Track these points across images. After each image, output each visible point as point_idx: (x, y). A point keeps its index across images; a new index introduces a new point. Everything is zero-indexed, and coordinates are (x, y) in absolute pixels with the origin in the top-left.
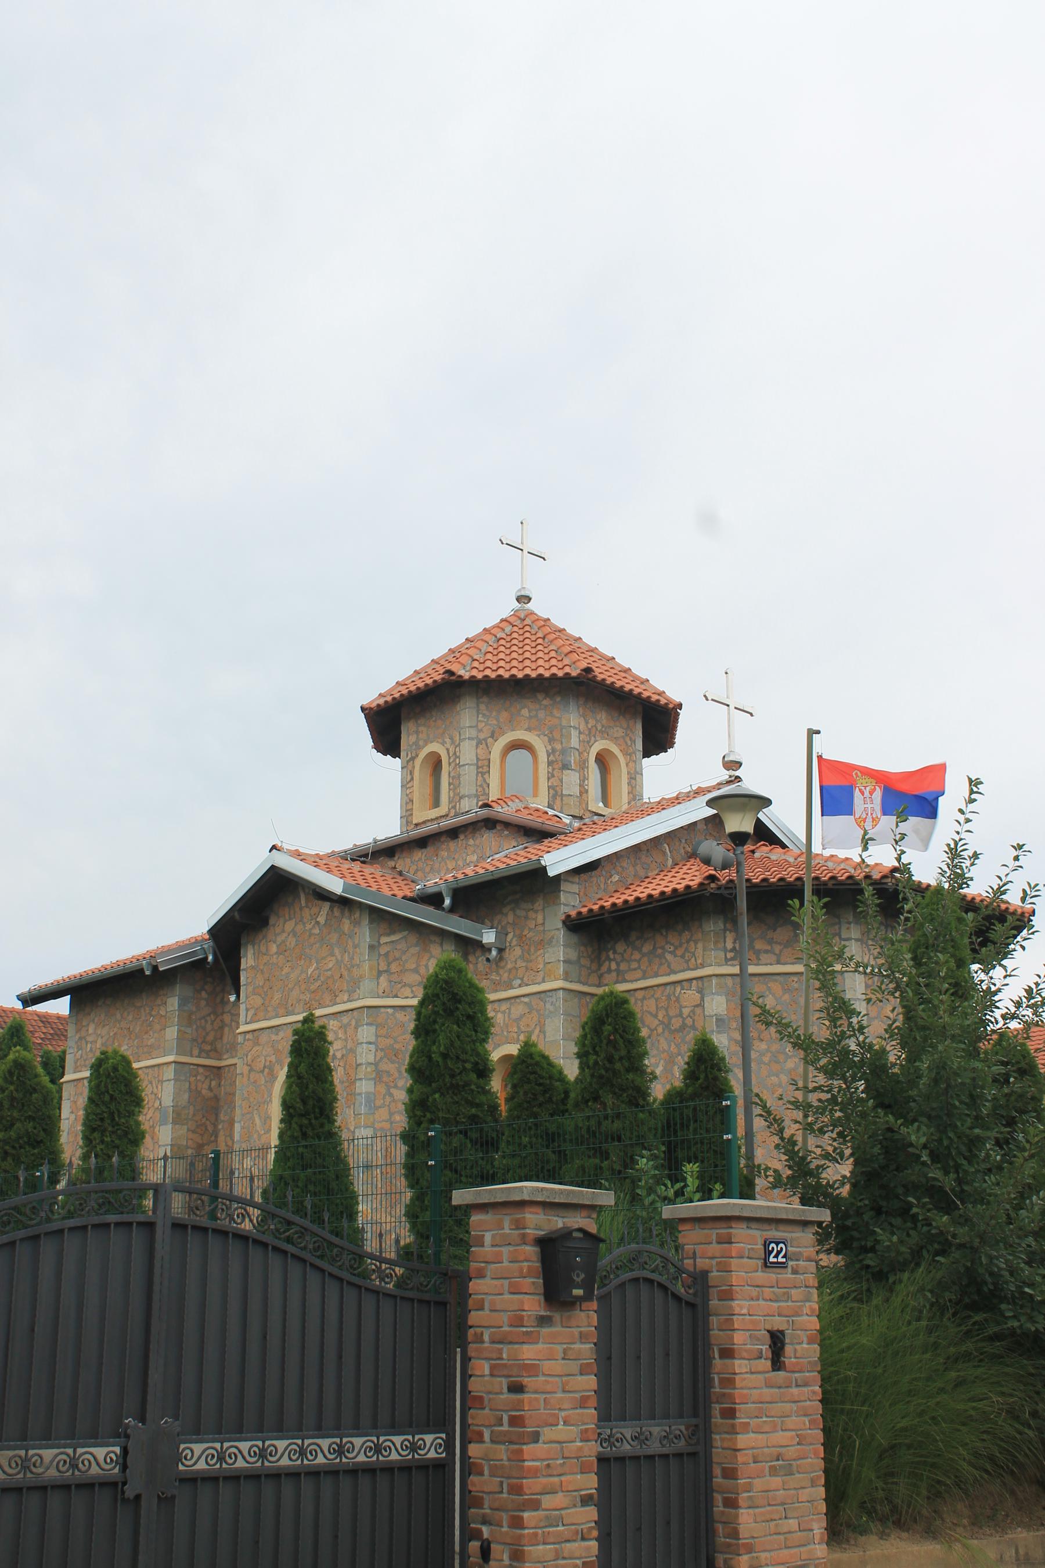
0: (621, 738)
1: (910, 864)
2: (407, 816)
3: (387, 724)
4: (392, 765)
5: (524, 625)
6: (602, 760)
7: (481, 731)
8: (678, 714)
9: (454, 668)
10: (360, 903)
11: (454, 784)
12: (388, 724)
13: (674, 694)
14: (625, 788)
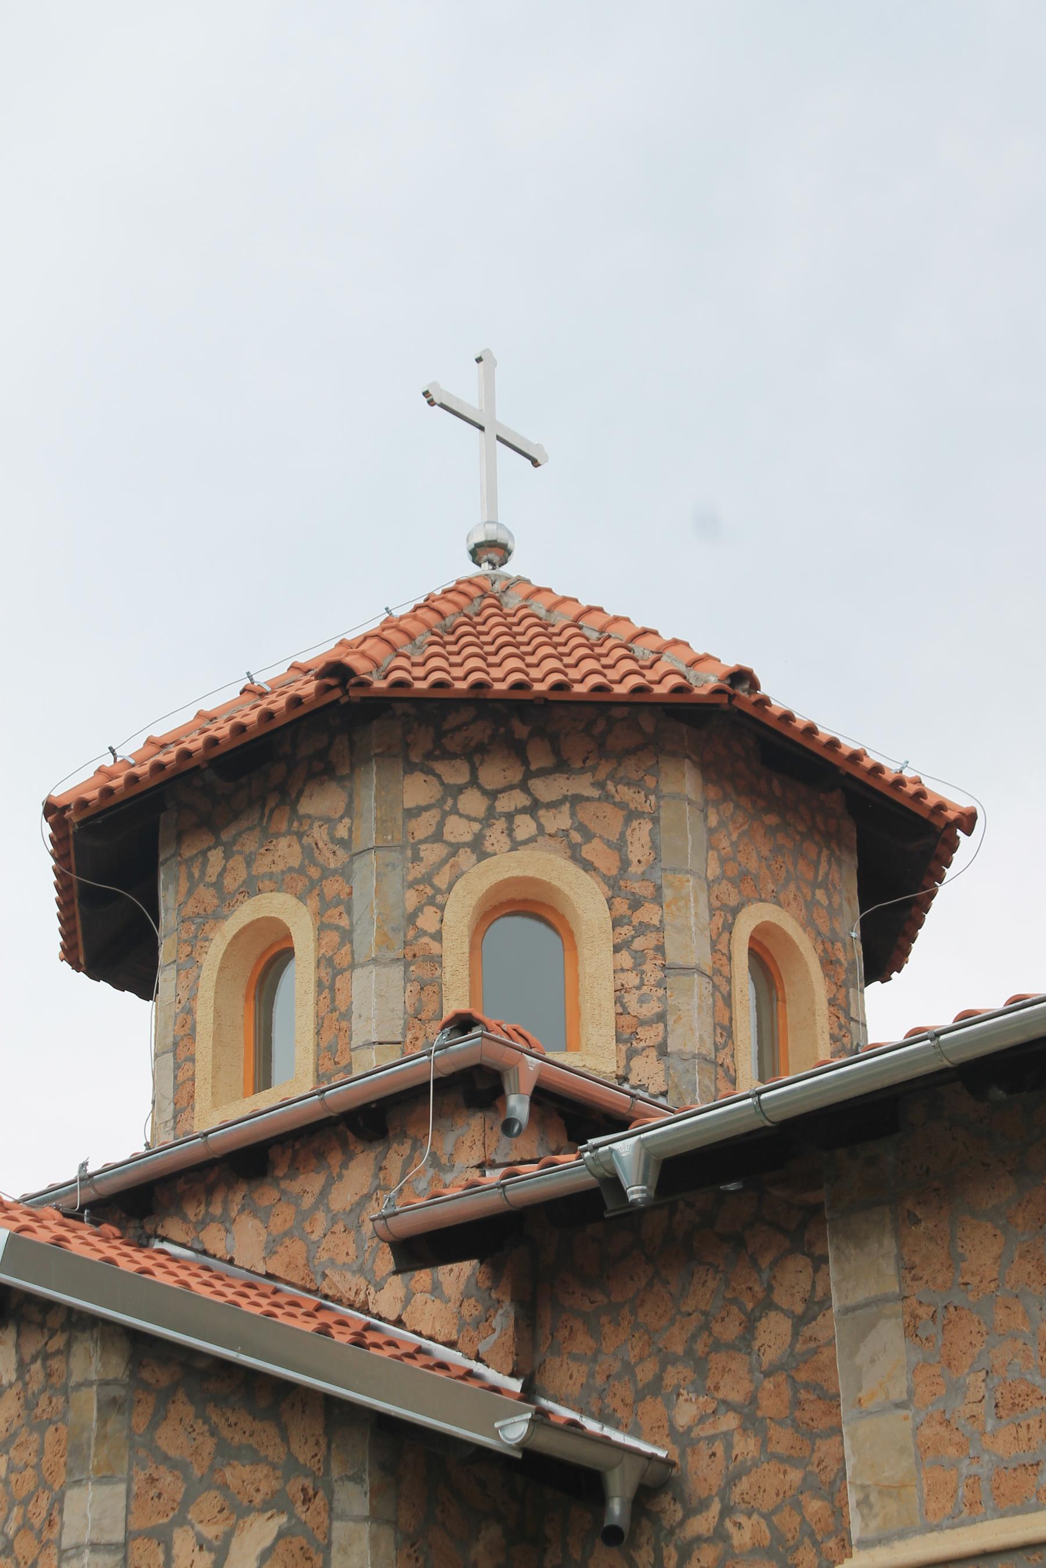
0: (811, 909)
1: (491, 551)
2: (177, 1091)
3: (118, 870)
4: (121, 1023)
5: (484, 599)
6: (766, 961)
7: (629, 1368)
8: (953, 846)
9: (359, 665)
10: (48, 1305)
11: (333, 1015)
12: (118, 870)
13: (946, 784)
14: (823, 1022)
